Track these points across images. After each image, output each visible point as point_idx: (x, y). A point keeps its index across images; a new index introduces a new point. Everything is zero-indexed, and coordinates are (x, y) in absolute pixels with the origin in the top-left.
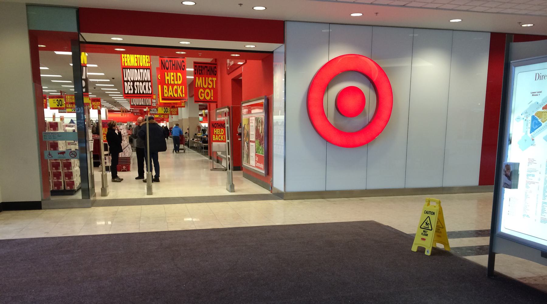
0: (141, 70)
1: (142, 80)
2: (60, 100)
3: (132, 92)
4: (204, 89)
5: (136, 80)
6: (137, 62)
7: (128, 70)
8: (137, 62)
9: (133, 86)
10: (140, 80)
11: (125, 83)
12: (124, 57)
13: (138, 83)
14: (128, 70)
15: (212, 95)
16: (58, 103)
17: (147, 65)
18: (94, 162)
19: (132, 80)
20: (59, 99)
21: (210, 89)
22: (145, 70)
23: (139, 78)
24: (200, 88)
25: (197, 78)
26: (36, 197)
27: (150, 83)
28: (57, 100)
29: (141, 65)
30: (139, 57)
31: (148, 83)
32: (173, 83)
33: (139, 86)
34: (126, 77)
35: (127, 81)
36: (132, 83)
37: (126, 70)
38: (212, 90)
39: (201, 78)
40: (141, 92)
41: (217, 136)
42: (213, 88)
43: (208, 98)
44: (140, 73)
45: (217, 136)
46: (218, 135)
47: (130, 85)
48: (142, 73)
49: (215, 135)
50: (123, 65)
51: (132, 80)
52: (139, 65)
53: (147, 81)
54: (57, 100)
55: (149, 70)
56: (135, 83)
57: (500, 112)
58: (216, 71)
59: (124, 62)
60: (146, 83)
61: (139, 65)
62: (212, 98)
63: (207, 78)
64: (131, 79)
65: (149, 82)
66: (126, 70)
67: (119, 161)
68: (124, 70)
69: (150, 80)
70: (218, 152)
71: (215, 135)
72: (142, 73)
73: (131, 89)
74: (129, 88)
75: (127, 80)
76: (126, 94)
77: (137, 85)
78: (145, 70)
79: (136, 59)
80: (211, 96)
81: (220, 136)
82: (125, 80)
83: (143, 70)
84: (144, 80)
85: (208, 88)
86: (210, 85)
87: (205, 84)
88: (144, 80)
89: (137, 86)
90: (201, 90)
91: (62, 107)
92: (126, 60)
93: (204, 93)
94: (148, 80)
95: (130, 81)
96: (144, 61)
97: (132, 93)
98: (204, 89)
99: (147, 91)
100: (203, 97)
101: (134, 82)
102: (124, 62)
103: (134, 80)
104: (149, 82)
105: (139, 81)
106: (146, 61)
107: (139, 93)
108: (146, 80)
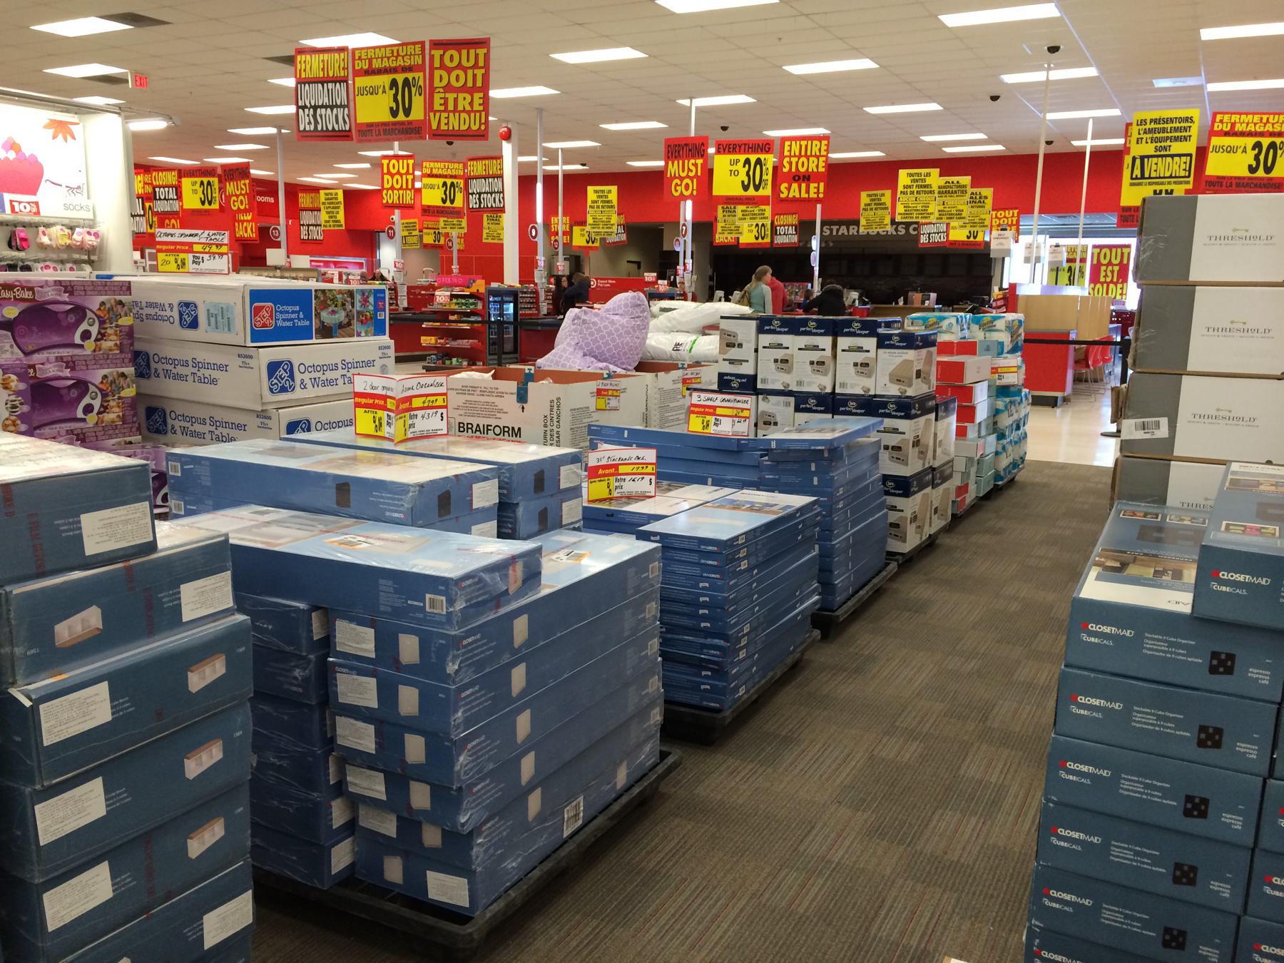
0: (330, 85)
2: (758, 161)
4: (682, 179)
5: (320, 104)
7: (307, 85)
8: (323, 69)
11: (301, 111)
13: (323, 110)
14: (307, 85)
15: (695, 188)
16: (445, 194)
17: (342, 74)
19: (313, 104)
20: (753, 158)
21: (691, 178)
22: (338, 84)
24: (675, 177)
25: (670, 163)
27: (346, 109)
28: (747, 161)
29: (331, 75)
36: (311, 110)
38: (695, 180)
42: (696, 175)
47: (308, 115)
51: (313, 104)
53: (498, 192)
54: (747, 161)
56: (319, 110)
57: (96, 940)
59: (300, 70)
63: (686, 161)
65: (500, 193)
70: (175, 197)
73: (310, 123)
74: (307, 121)
78: (338, 84)
80: (693, 190)
85: (688, 176)
86: (692, 171)
87: (683, 171)
89: (321, 116)
90: (234, 198)
92: (303, 68)
93: (681, 185)
97: (312, 129)
98: (682, 179)
99: (341, 126)
100: (679, 192)
102: (300, 70)
104: (500, 193)
105: (487, 193)
107: (325, 129)
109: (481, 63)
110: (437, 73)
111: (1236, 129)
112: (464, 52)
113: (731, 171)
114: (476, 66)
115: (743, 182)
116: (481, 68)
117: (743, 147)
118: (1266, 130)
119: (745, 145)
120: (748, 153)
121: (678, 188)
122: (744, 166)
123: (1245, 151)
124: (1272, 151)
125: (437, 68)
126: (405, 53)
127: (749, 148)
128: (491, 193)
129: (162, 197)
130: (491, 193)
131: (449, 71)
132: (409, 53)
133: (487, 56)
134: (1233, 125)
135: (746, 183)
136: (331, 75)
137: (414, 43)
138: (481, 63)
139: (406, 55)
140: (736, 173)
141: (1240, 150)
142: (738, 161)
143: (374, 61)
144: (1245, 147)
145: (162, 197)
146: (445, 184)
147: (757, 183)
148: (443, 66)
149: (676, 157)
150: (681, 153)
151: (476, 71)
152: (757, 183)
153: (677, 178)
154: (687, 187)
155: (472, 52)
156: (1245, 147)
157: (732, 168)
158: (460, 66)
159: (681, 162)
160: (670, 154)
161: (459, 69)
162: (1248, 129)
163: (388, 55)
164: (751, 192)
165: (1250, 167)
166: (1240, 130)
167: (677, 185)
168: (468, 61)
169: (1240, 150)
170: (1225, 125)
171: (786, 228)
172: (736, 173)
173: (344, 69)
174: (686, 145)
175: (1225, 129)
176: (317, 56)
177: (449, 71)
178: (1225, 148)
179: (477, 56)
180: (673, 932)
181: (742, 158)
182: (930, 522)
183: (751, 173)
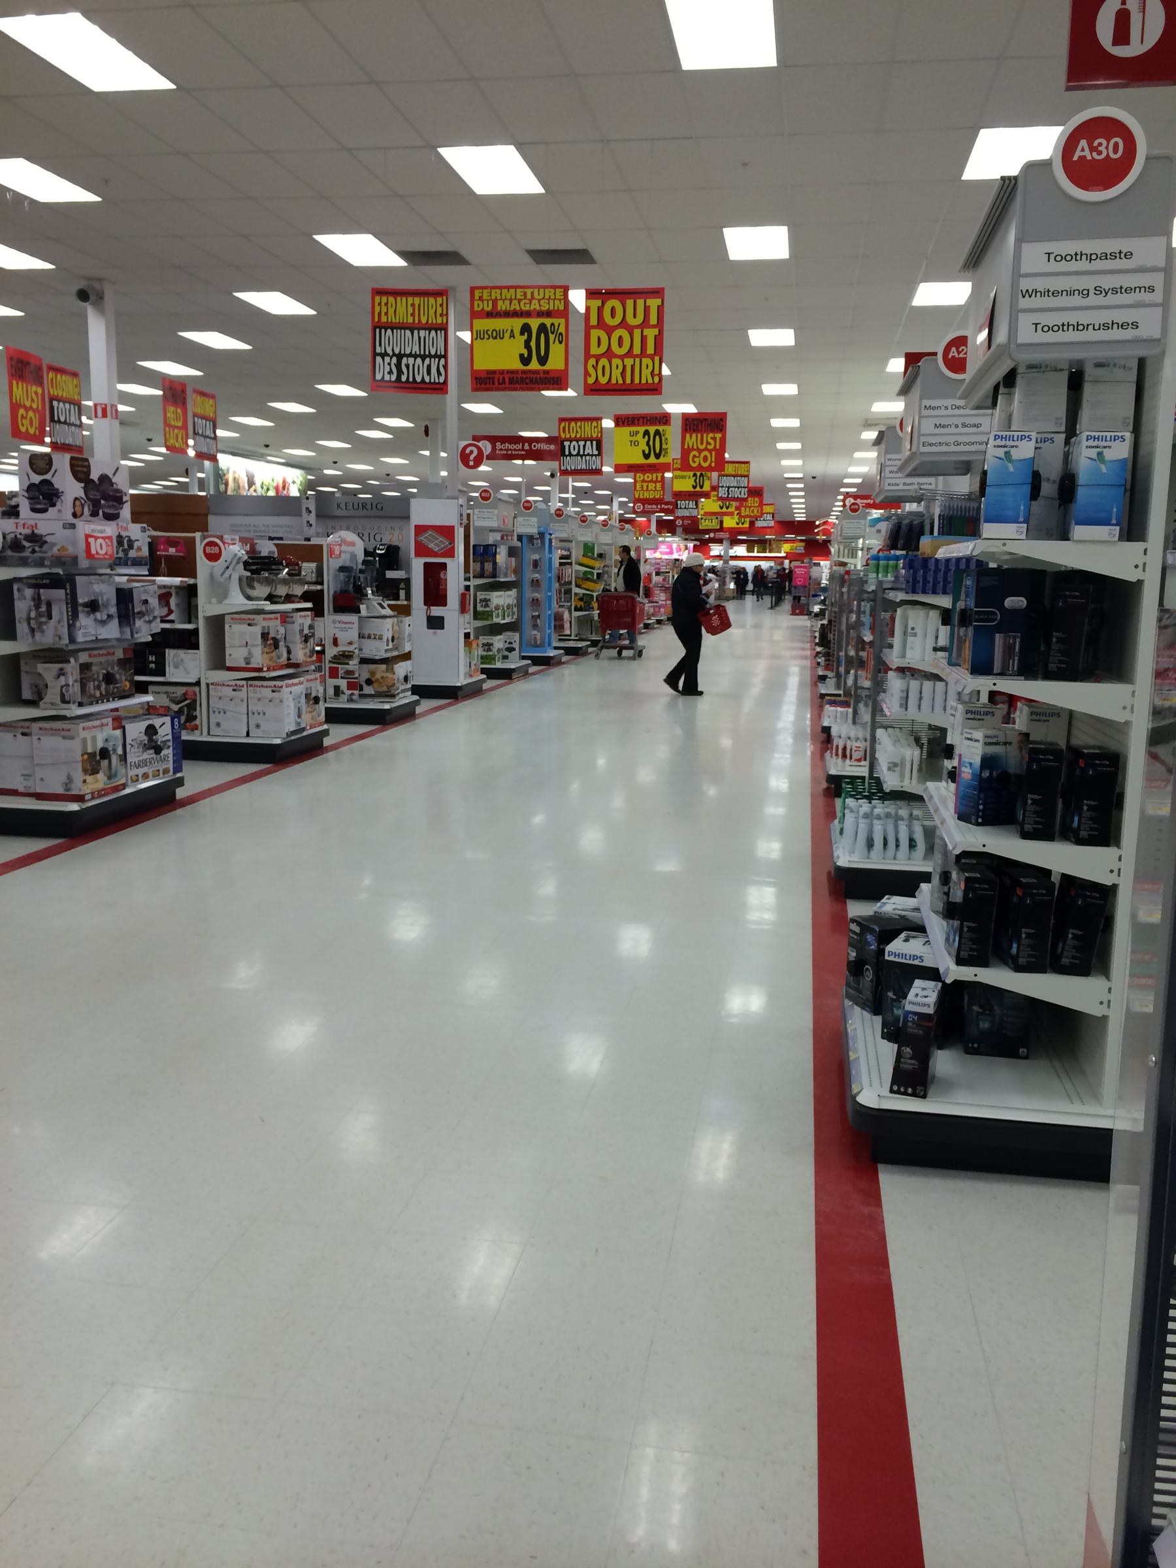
0: (422, 333)
1: (422, 353)
2: (657, 433)
3: (394, 377)
4: (700, 451)
5: (408, 352)
6: (413, 315)
7: (389, 331)
8: (413, 315)
9: (398, 366)
10: (418, 353)
11: (379, 359)
12: (380, 304)
13: (411, 360)
14: (389, 331)
15: (713, 460)
17: (439, 320)
19: (397, 352)
20: (652, 429)
21: (710, 451)
22: (433, 332)
23: (416, 349)
24: (693, 449)
26: (461, 680)
28: (646, 433)
29: (424, 320)
30: (419, 305)
31: (437, 360)
32: (764, 503)
33: (414, 365)
34: (380, 345)
37: (383, 331)
40: (419, 379)
43: (705, 465)
47: (389, 364)
50: (376, 320)
51: (397, 352)
52: (417, 321)
53: (436, 356)
54: (646, 433)
58: (722, 425)
59: (380, 314)
60: (433, 359)
61: (417, 321)
62: (713, 465)
63: (705, 435)
65: (440, 357)
66: (383, 331)
68: (378, 330)
69: (443, 353)
72: (425, 338)
73: (390, 372)
74: (387, 369)
78: (433, 332)
79: (410, 310)
80: (712, 462)
83: (427, 332)
85: (706, 449)
87: (702, 444)
89: (407, 366)
90: (694, 453)
92: (384, 309)
93: (699, 457)
94: (439, 353)
95: (391, 354)
96: (432, 312)
98: (700, 451)
101: (400, 357)
103: (402, 352)
104: (440, 357)
105: (415, 356)
107: (411, 380)
108: (433, 353)
109: (653, 320)
113: (631, 441)
114: (645, 324)
115: (644, 451)
116: (653, 327)
117: (641, 420)
120: (647, 425)
122: (644, 437)
123: (512, 336)
124: (543, 335)
125: (594, 327)
126: (541, 296)
127: (647, 420)
129: (574, 453)
130: (423, 358)
131: (609, 330)
132: (547, 297)
133: (660, 309)
134: (495, 302)
135: (647, 452)
136: (424, 320)
138: (653, 320)
139: (544, 298)
140: (636, 444)
141: (507, 335)
142: (637, 432)
143: (500, 303)
144: (512, 331)
146: (526, 329)
147: (657, 451)
148: (601, 324)
149: (694, 430)
150: (700, 426)
151: (646, 332)
152: (657, 451)
153: (695, 450)
156: (512, 331)
157: (631, 439)
158: (623, 324)
159: (699, 435)
160: (688, 428)
163: (518, 297)
164: (652, 460)
168: (635, 316)
169: (507, 335)
171: (582, 443)
172: (636, 443)
173: (441, 315)
174: (705, 420)
175: (486, 309)
177: (609, 330)
178: (490, 333)
179: (647, 310)
180: (109, 650)
181: (642, 429)
183: (651, 443)
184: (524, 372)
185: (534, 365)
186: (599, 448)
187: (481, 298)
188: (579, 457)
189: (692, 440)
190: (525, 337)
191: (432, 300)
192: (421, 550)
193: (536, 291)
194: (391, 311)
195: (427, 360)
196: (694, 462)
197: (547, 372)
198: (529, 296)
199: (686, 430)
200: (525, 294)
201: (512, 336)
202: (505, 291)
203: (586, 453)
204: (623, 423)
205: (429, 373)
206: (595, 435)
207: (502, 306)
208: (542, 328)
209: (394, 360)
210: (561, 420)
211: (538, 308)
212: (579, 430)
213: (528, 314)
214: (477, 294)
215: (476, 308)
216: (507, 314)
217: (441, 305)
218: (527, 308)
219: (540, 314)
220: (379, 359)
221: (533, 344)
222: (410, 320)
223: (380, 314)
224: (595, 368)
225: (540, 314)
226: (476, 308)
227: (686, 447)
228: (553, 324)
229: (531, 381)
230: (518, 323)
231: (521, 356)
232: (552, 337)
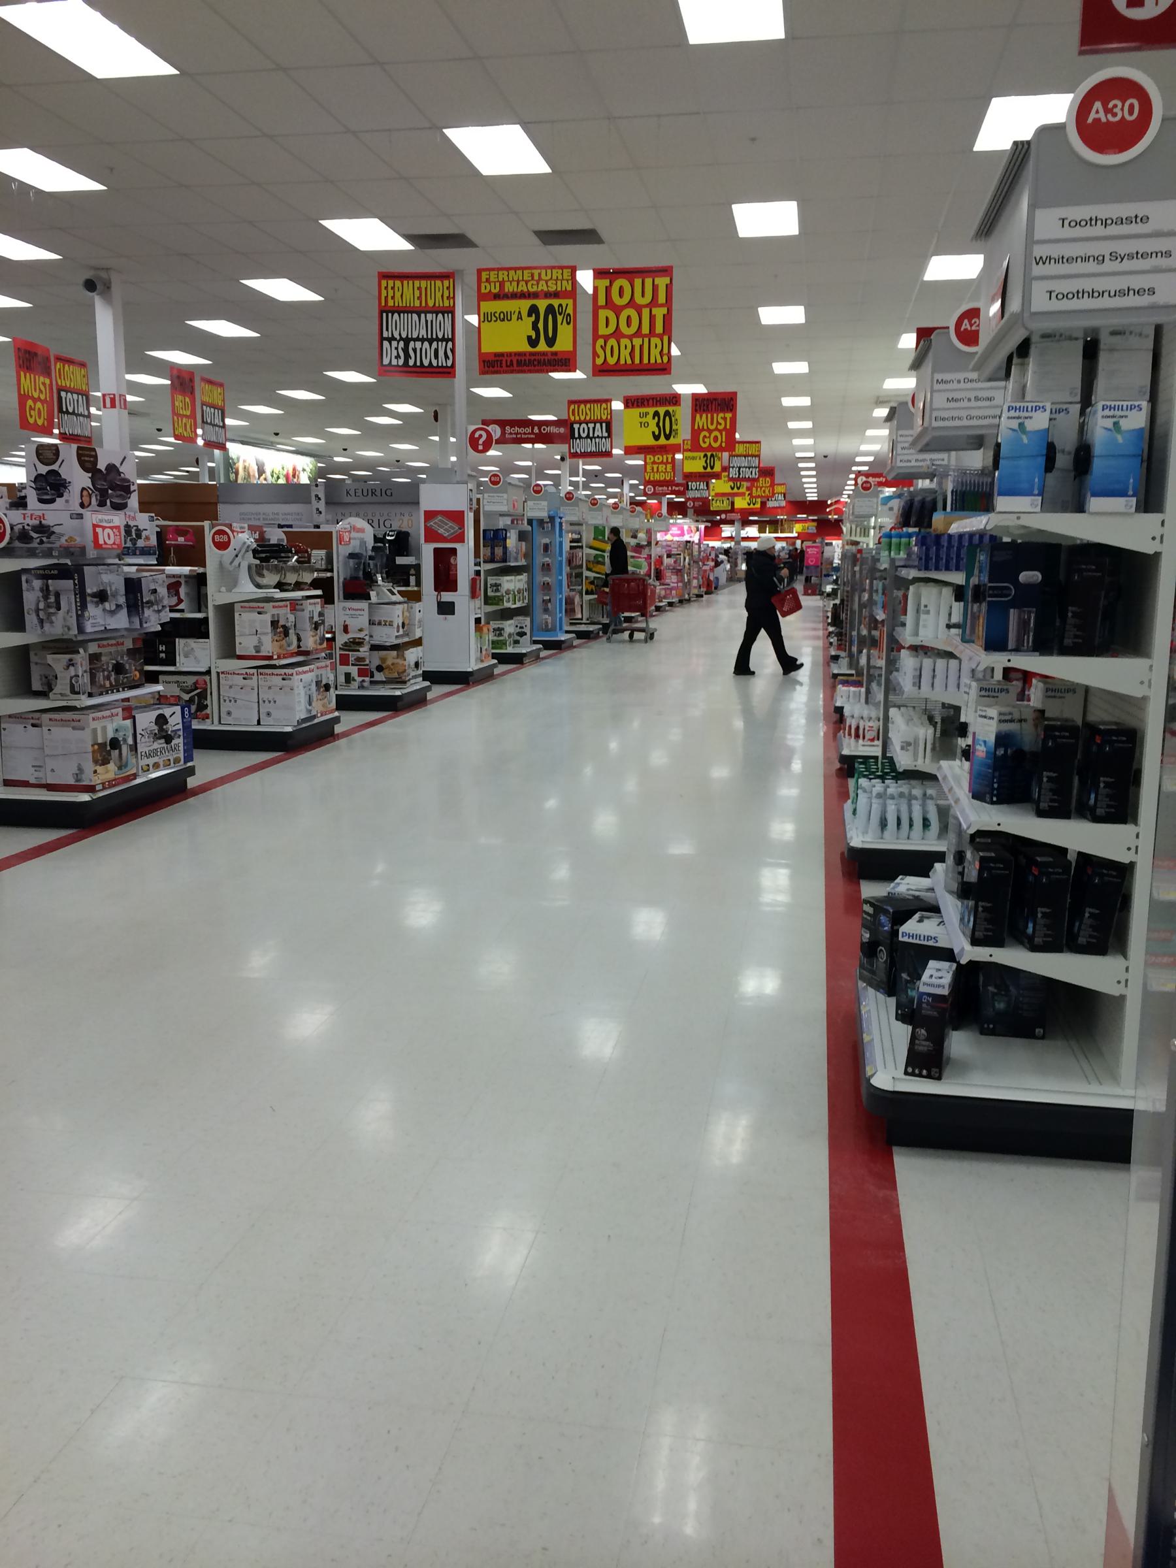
0: (429, 316)
1: (429, 337)
2: (667, 413)
3: (401, 362)
4: (710, 431)
5: (415, 336)
6: (420, 298)
8: (420, 298)
10: (425, 337)
11: (386, 344)
12: (386, 288)
13: (418, 344)
14: (396, 315)
15: (724, 439)
17: (446, 304)
18: (578, 482)
19: (404, 336)
21: (720, 431)
22: (440, 316)
23: (423, 333)
24: (703, 430)
27: (450, 344)
28: (656, 414)
29: (431, 304)
31: (444, 343)
33: (421, 349)
35: (390, 340)
37: (390, 315)
38: (724, 433)
39: (704, 416)
40: (426, 363)
41: (759, 489)
44: (427, 321)
45: (759, 489)
46: (761, 488)
47: (397, 348)
48: (432, 321)
49: (757, 488)
50: (383, 304)
51: (404, 336)
53: (443, 339)
54: (656, 414)
55: (450, 315)
58: (733, 405)
59: (386, 298)
60: (440, 343)
62: (724, 445)
63: (715, 415)
64: (400, 334)
65: (447, 340)
66: (390, 315)
67: (974, 488)
68: (384, 315)
69: (450, 337)
71: (757, 488)
72: (432, 321)
73: (398, 357)
74: (395, 353)
75: (390, 336)
76: (385, 366)
77: (416, 349)
78: (440, 316)
79: (417, 293)
80: (722, 442)
81: (763, 489)
82: (385, 334)
83: (434, 315)
84: (434, 337)
85: (716, 429)
86: (721, 424)
87: (712, 424)
88: (434, 337)
89: (415, 350)
91: (672, 441)
93: (709, 437)
94: (446, 337)
96: (439, 295)
98: (710, 431)
101: (407, 341)
103: (410, 336)
104: (447, 340)
105: (423, 340)
106: (442, 296)
107: (418, 364)
108: (440, 336)
109: (662, 299)
110: (603, 314)
111: (506, 290)
112: (638, 282)
113: (641, 423)
114: (654, 303)
116: (662, 306)
118: (540, 289)
119: (653, 399)
120: (657, 406)
121: (706, 440)
122: (654, 418)
125: (602, 307)
128: (431, 341)
129: (584, 435)
130: (431, 341)
131: (618, 311)
132: (554, 277)
133: (669, 288)
134: (502, 284)
135: (657, 433)
136: (431, 304)
137: (562, 268)
138: (662, 299)
140: (646, 425)
141: (515, 317)
142: (647, 414)
143: (507, 285)
145: (584, 435)
146: (533, 310)
148: (609, 304)
149: (704, 410)
151: (655, 311)
154: (716, 439)
155: (649, 281)
158: (632, 303)
159: (709, 415)
160: (698, 408)
161: (632, 307)
162: (519, 290)
164: (662, 441)
165: (704, 467)
166: (511, 290)
167: (705, 437)
168: (643, 295)
169: (515, 317)
170: (493, 285)
171: (591, 426)
172: (646, 425)
173: (448, 298)
174: (715, 399)
175: (493, 291)
176: (411, 282)
179: (655, 288)
181: (651, 411)
182: (360, 610)
184: (531, 354)
185: (542, 346)
186: (609, 430)
187: (488, 280)
188: (589, 440)
189: (702, 420)
190: (533, 318)
191: (438, 283)
192: (431, 536)
193: (543, 272)
194: (398, 295)
195: (435, 344)
196: (704, 442)
197: (555, 353)
198: (536, 277)
199: (696, 411)
200: (532, 276)
201: (520, 318)
202: (512, 273)
203: (596, 435)
204: (633, 405)
205: (436, 356)
206: (604, 417)
207: (509, 288)
208: (550, 309)
209: (402, 344)
210: (571, 402)
211: (545, 289)
212: (588, 412)
213: (535, 295)
214: (484, 275)
215: (483, 291)
216: (514, 296)
217: (448, 288)
218: (535, 289)
219: (548, 295)
220: (386, 344)
221: (541, 325)
222: (417, 304)
223: (386, 298)
224: (603, 348)
225: (548, 295)
226: (483, 291)
227: (696, 427)
228: (560, 305)
229: (539, 362)
230: (525, 305)
231: (529, 338)
232: (560, 318)
